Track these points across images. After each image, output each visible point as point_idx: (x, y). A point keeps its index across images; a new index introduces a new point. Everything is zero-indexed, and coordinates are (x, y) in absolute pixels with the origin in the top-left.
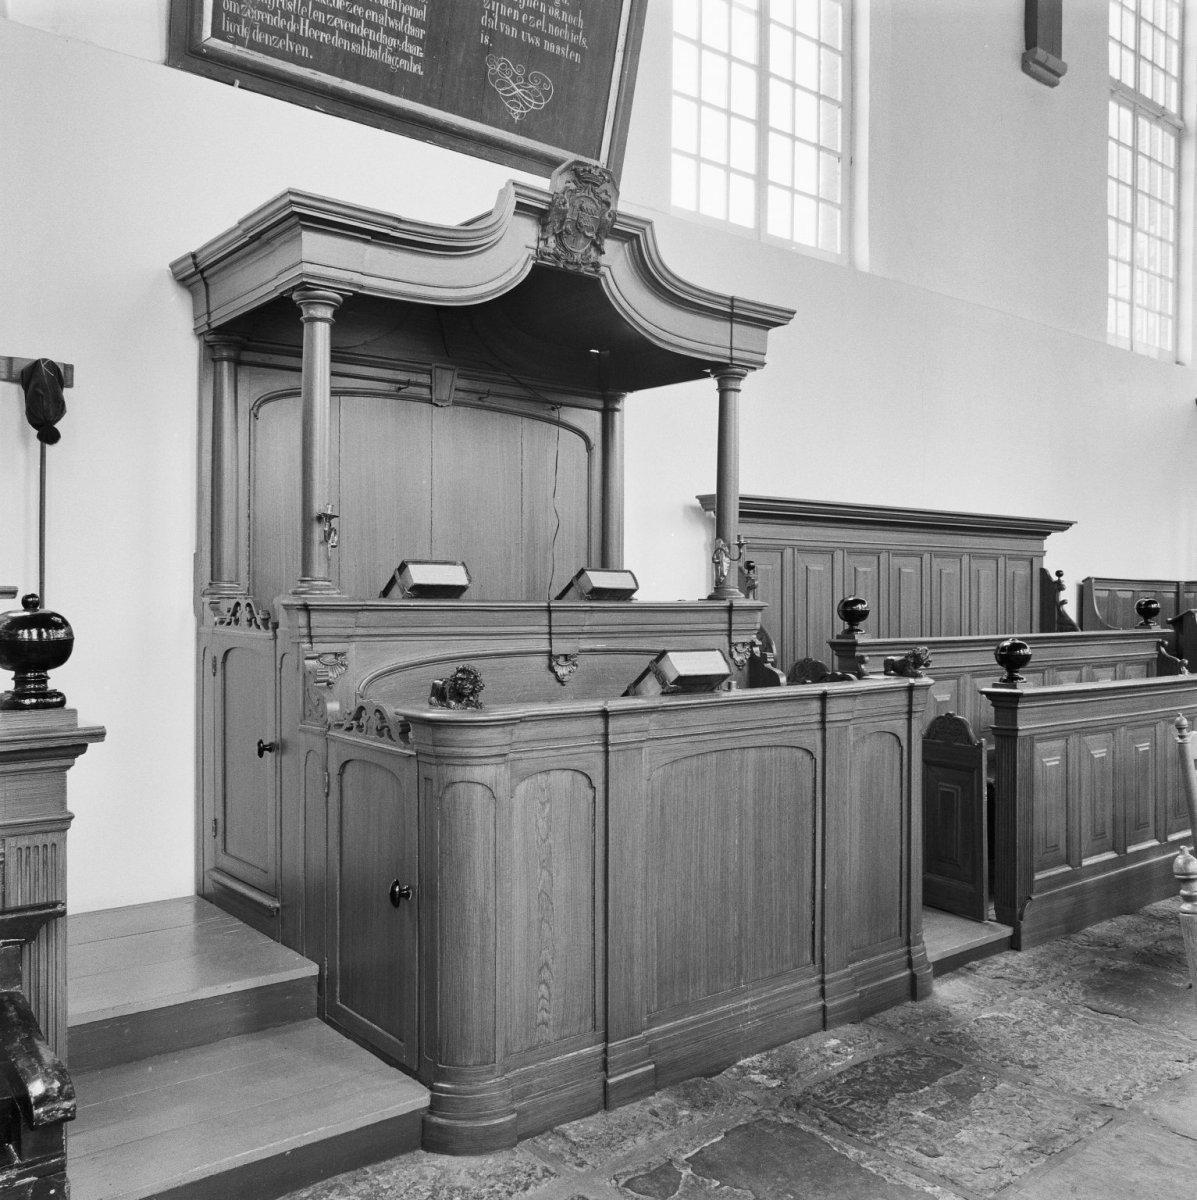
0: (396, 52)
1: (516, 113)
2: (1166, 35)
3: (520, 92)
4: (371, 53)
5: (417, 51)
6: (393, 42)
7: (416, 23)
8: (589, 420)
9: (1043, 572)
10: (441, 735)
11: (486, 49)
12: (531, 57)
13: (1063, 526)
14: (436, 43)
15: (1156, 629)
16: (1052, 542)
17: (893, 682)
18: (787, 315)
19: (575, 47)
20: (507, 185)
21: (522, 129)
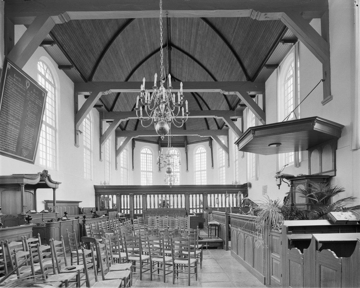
0: (13, 149)
1: (25, 155)
2: (89, 139)
3: (25, 153)
4: (11, 149)
5: (15, 149)
6: (13, 148)
7: (15, 146)
8: (32, 191)
9: (79, 207)
10: (50, 225)
11: (22, 148)
12: (27, 149)
13: (81, 202)
14: (17, 148)
15: (93, 213)
16: (80, 204)
17: (76, 219)
18: (61, 183)
19: (31, 148)
20: (39, 173)
21: (25, 157)
